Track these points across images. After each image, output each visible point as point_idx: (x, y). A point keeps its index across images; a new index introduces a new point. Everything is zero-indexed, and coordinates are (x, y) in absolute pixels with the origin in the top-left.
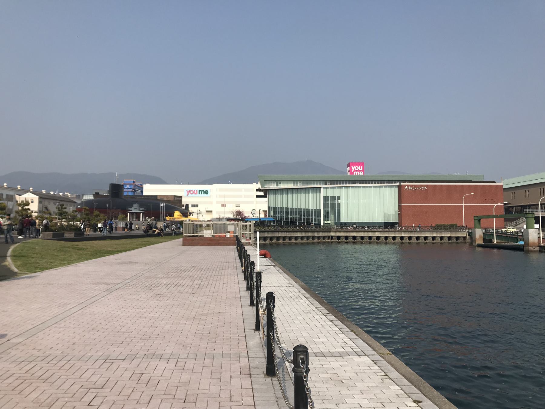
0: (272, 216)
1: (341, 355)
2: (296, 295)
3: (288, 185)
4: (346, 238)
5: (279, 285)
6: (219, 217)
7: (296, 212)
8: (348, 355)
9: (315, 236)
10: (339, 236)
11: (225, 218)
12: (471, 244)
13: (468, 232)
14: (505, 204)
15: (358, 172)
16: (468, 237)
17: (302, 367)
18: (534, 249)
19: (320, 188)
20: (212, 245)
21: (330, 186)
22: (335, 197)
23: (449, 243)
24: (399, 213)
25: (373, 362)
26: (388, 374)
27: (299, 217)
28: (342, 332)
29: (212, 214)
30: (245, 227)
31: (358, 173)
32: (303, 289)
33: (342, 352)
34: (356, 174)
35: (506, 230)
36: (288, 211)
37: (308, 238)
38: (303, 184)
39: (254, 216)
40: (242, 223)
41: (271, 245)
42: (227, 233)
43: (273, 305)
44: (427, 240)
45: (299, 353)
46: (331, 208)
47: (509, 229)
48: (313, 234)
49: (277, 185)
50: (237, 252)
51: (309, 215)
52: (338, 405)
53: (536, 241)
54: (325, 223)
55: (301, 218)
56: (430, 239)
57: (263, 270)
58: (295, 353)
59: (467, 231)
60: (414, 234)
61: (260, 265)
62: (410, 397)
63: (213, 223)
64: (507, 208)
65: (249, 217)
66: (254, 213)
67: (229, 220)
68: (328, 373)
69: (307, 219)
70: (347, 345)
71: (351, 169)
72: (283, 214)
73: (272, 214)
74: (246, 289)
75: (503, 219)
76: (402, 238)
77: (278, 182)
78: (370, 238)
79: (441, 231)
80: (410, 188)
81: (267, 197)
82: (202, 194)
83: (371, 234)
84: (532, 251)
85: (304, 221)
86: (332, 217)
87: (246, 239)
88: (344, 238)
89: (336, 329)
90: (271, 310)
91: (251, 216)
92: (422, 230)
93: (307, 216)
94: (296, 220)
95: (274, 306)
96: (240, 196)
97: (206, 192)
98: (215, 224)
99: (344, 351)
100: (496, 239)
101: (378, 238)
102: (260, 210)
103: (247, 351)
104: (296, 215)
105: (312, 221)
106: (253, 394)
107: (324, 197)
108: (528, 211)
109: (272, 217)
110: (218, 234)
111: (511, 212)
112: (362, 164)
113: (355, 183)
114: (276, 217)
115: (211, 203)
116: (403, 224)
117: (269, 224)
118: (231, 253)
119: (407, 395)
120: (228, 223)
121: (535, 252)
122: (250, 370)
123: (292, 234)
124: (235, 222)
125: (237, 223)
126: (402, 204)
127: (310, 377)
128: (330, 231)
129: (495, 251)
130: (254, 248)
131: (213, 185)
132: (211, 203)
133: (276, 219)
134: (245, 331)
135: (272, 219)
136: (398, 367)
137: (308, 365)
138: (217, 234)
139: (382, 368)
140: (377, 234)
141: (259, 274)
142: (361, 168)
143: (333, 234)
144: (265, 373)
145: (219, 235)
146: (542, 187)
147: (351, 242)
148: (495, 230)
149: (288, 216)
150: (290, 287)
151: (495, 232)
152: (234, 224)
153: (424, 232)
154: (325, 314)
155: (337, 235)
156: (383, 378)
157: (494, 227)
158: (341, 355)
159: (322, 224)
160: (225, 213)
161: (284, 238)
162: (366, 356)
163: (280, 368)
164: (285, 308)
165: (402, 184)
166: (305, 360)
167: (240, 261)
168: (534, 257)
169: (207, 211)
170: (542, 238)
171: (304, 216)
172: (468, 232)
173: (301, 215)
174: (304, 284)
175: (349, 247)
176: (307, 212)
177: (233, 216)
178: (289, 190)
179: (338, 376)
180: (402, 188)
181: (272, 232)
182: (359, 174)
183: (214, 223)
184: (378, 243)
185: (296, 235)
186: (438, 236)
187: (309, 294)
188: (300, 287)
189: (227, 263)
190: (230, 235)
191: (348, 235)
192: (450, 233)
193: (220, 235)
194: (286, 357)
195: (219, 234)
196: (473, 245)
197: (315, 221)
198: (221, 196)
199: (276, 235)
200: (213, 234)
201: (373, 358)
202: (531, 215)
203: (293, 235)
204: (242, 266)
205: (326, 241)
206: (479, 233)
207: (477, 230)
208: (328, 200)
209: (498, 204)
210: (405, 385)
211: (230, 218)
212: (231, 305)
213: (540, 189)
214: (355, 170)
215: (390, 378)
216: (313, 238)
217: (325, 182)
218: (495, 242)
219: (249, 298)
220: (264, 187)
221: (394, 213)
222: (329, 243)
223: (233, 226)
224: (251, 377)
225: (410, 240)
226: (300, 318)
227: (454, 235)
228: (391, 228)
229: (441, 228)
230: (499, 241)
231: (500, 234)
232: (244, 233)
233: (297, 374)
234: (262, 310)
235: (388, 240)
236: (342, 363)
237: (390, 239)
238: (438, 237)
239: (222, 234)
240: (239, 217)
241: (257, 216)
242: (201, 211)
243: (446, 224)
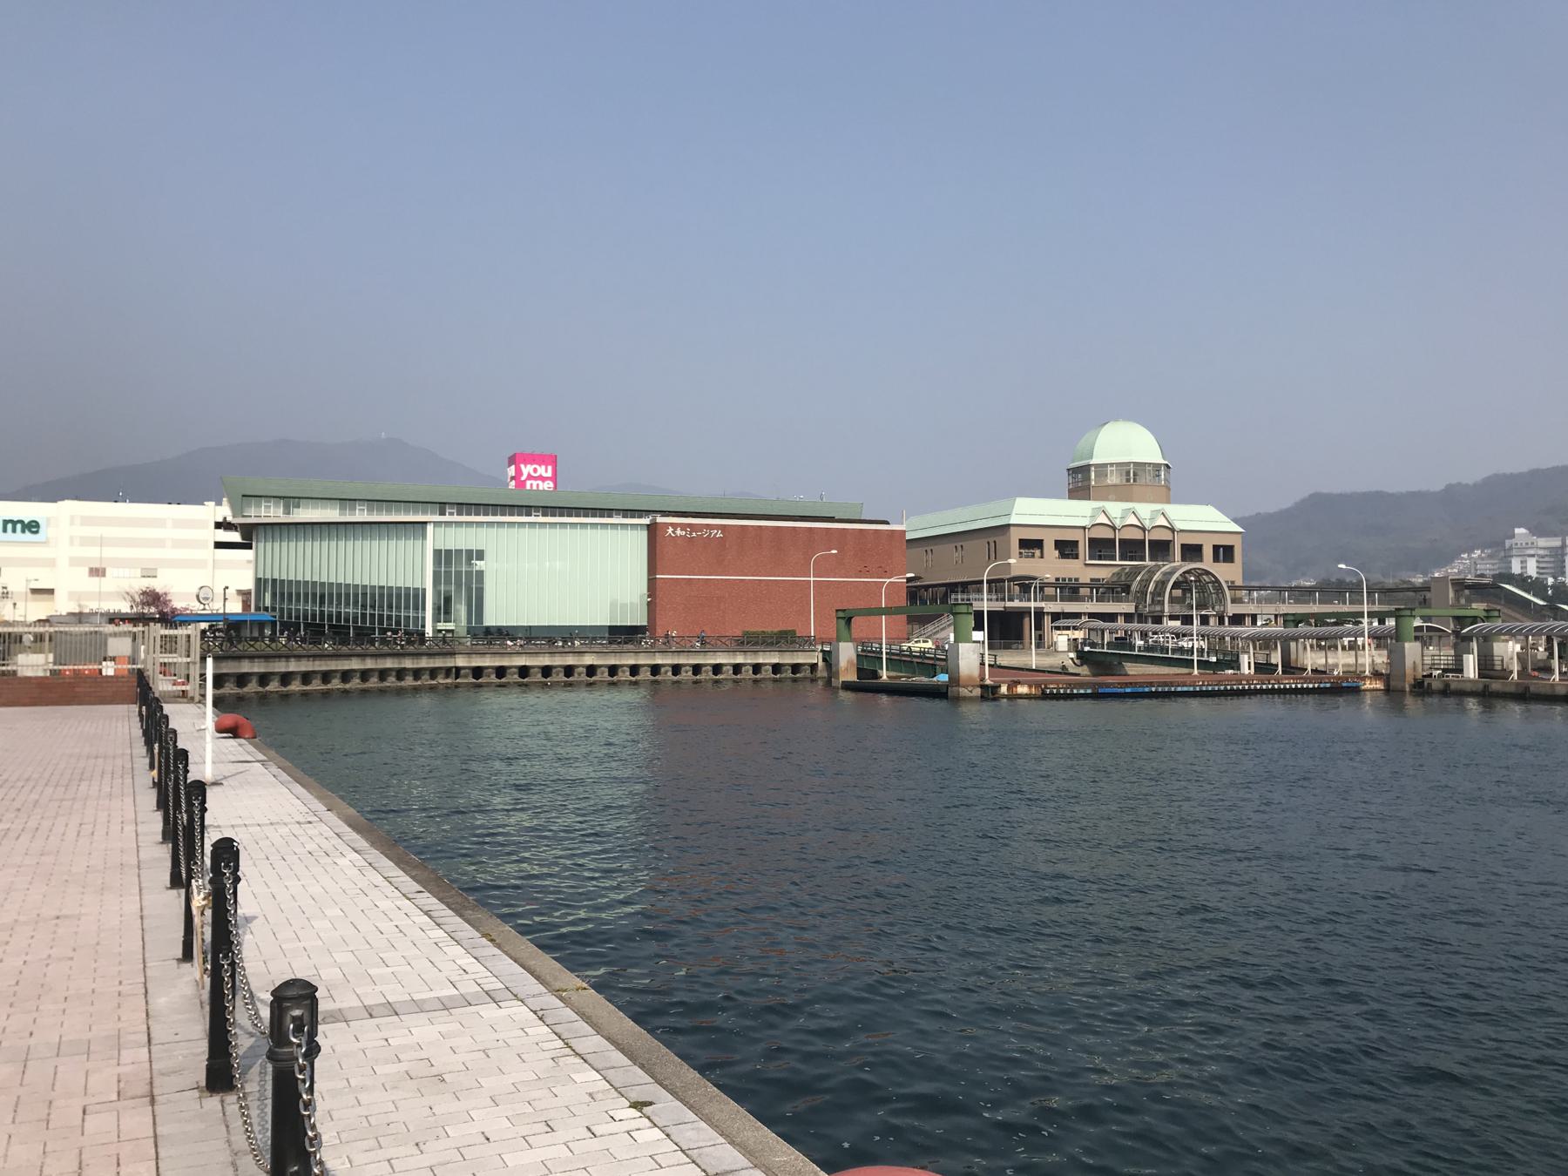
0: (266, 609)
1: (445, 1006)
2: (326, 845)
3: (324, 511)
4: (501, 671)
5: (274, 819)
6: (77, 611)
7: (348, 595)
8: (466, 1004)
9: (405, 668)
10: (479, 667)
11: (102, 614)
12: (828, 682)
13: (822, 651)
14: (909, 580)
15: (540, 482)
16: (821, 664)
17: (294, 1043)
18: (971, 692)
19: (426, 523)
20: (42, 704)
21: (456, 518)
22: (470, 552)
23: (775, 681)
24: (649, 599)
25: (536, 1014)
26: (573, 1043)
27: (372, 612)
28: (456, 941)
29: (53, 600)
30: (169, 644)
31: (538, 485)
32: (350, 826)
33: (450, 998)
34: (535, 488)
35: (909, 645)
36: (321, 593)
37: (383, 674)
38: (370, 510)
39: (207, 607)
40: (159, 630)
41: (263, 698)
42: (104, 663)
43: (231, 877)
44: (780, 672)
45: (289, 1004)
46: (458, 585)
47: (916, 642)
48: (400, 663)
49: (287, 512)
50: (140, 724)
51: (390, 607)
52: (421, 1145)
53: (976, 673)
54: (439, 628)
55: (364, 615)
56: (707, 672)
57: (225, 778)
58: (276, 1005)
59: (820, 648)
60: (688, 659)
61: (214, 762)
62: (623, 1096)
63: (52, 630)
64: (914, 589)
65: (187, 609)
66: (207, 599)
67: (114, 618)
68: (402, 1060)
69: (381, 616)
70: (466, 977)
71: (519, 472)
72: (306, 601)
73: (268, 602)
74: (160, 838)
75: (904, 617)
76: (655, 669)
77: (290, 501)
78: (569, 670)
79: (754, 648)
80: (679, 532)
81: (251, 548)
82: (14, 531)
83: (570, 660)
84: (965, 698)
85: (372, 622)
86: (461, 610)
87: (172, 682)
88: (563, 670)
89: (441, 933)
90: (227, 891)
91: (196, 607)
92: (708, 646)
93: (381, 607)
94: (347, 620)
95: (237, 880)
96: (160, 543)
97: (32, 527)
98: (61, 632)
99: (456, 992)
100: (887, 670)
101: (591, 670)
102: (227, 588)
103: (145, 1027)
104: (347, 604)
105: (398, 623)
106: (157, 1153)
107: (437, 553)
108: (959, 597)
109: (268, 611)
110: (71, 667)
111: (923, 602)
112: (550, 460)
113: (529, 514)
114: (282, 610)
115: (51, 563)
116: (660, 632)
117: (256, 634)
118: (116, 727)
119: (616, 1093)
120: (111, 628)
121: (971, 699)
122: (151, 1083)
123: (334, 662)
124: (135, 626)
125: (140, 628)
126: (658, 576)
127: (347, 1080)
128: (452, 654)
129: (884, 699)
130: (199, 708)
131: (60, 503)
132: (51, 563)
133: (282, 616)
134: (145, 966)
135: (267, 616)
136: (600, 1022)
137: (317, 1035)
138: (66, 667)
139: (558, 1029)
140: (589, 660)
141: (199, 788)
142: (546, 471)
143: (461, 662)
144: (203, 1083)
145: (74, 670)
146: (961, 544)
147: (515, 683)
148: (884, 646)
149: (320, 607)
150: (310, 822)
151: (884, 650)
152: (130, 632)
153: (712, 653)
154: (410, 896)
155: (474, 664)
156: (559, 1055)
157: (882, 639)
158: (445, 1006)
159: (429, 631)
160: (100, 596)
161: (306, 677)
162: (518, 1000)
163: (255, 1063)
164: (286, 887)
165: (660, 520)
166: (305, 1022)
167: (147, 751)
168: (975, 714)
169: (35, 591)
170: (990, 665)
171: (373, 607)
172: (822, 651)
173: (364, 606)
174: (355, 812)
175: (512, 699)
176: (382, 596)
177: (132, 606)
178: (309, 529)
179: (432, 1065)
180: (658, 532)
181: (267, 658)
182: (541, 488)
183: (57, 629)
184: (590, 684)
185: (346, 668)
186: (749, 661)
187: (367, 840)
188: (342, 821)
189: (100, 761)
190: (115, 670)
191: (505, 662)
192: (777, 653)
193: (79, 670)
194: (259, 1025)
195: (76, 667)
196: (833, 684)
197: (407, 625)
198: (86, 541)
199: (280, 667)
200: (51, 666)
201: (536, 1003)
202: (966, 607)
203: (337, 666)
204: (152, 767)
205: (441, 681)
206: (847, 653)
207: (842, 645)
208: (448, 563)
209: (892, 580)
210: (615, 1065)
211: (119, 613)
212: (103, 889)
213: (988, 543)
214: (530, 477)
215: (577, 1054)
216: (400, 674)
217: (442, 507)
218: (884, 675)
219: (169, 864)
220: (244, 516)
221: (636, 600)
222: (447, 687)
223: (129, 640)
224: (153, 1102)
225: (633, 676)
226: (334, 912)
227: (788, 659)
228: (626, 643)
229: (756, 640)
230: (893, 674)
231: (897, 655)
232: (166, 660)
233: (280, 1064)
234: (202, 896)
235: (741, 673)
236: (444, 1028)
237: (624, 672)
238: (749, 664)
239: (85, 667)
240: (153, 610)
241: (216, 606)
242: (9, 589)
243: (769, 630)
